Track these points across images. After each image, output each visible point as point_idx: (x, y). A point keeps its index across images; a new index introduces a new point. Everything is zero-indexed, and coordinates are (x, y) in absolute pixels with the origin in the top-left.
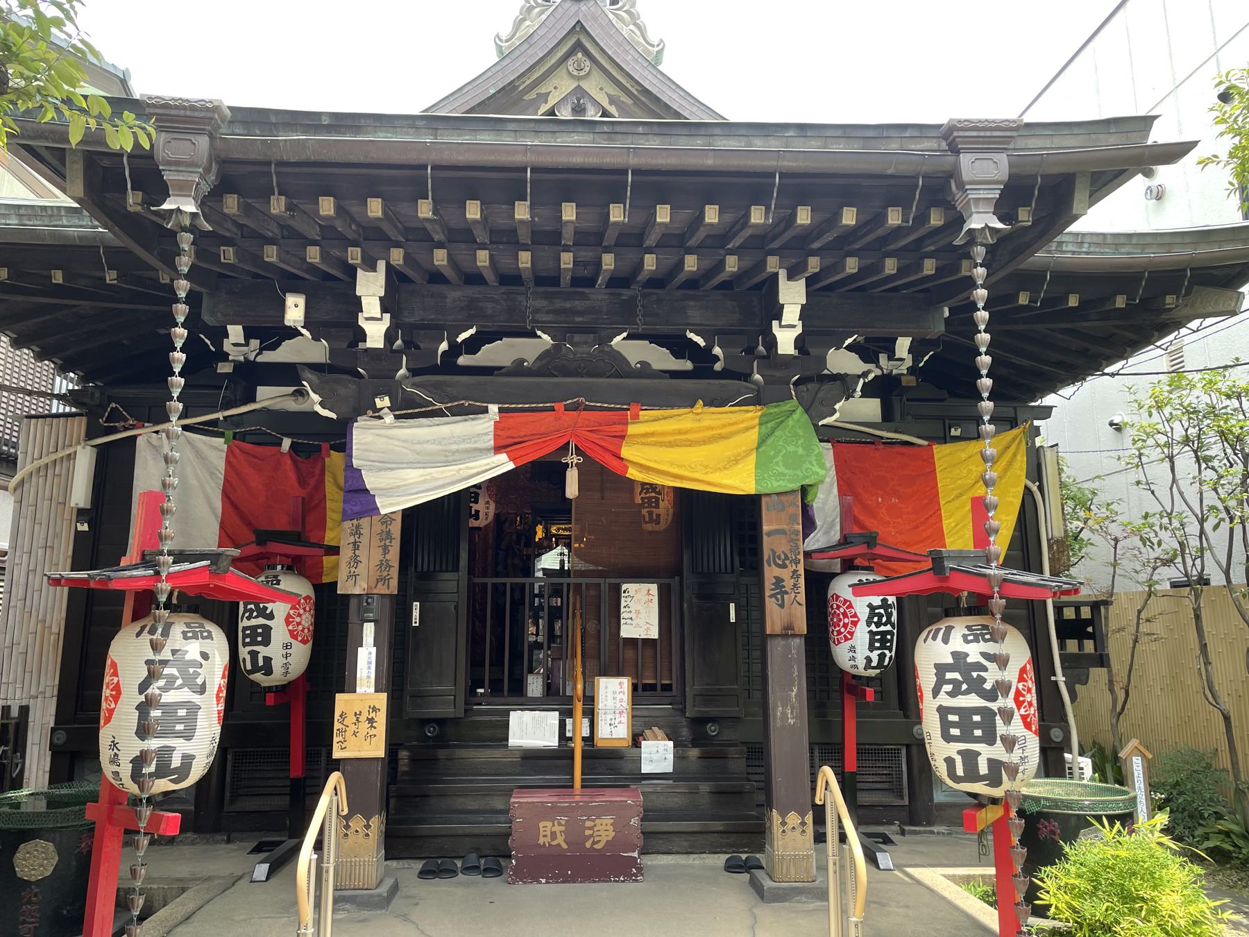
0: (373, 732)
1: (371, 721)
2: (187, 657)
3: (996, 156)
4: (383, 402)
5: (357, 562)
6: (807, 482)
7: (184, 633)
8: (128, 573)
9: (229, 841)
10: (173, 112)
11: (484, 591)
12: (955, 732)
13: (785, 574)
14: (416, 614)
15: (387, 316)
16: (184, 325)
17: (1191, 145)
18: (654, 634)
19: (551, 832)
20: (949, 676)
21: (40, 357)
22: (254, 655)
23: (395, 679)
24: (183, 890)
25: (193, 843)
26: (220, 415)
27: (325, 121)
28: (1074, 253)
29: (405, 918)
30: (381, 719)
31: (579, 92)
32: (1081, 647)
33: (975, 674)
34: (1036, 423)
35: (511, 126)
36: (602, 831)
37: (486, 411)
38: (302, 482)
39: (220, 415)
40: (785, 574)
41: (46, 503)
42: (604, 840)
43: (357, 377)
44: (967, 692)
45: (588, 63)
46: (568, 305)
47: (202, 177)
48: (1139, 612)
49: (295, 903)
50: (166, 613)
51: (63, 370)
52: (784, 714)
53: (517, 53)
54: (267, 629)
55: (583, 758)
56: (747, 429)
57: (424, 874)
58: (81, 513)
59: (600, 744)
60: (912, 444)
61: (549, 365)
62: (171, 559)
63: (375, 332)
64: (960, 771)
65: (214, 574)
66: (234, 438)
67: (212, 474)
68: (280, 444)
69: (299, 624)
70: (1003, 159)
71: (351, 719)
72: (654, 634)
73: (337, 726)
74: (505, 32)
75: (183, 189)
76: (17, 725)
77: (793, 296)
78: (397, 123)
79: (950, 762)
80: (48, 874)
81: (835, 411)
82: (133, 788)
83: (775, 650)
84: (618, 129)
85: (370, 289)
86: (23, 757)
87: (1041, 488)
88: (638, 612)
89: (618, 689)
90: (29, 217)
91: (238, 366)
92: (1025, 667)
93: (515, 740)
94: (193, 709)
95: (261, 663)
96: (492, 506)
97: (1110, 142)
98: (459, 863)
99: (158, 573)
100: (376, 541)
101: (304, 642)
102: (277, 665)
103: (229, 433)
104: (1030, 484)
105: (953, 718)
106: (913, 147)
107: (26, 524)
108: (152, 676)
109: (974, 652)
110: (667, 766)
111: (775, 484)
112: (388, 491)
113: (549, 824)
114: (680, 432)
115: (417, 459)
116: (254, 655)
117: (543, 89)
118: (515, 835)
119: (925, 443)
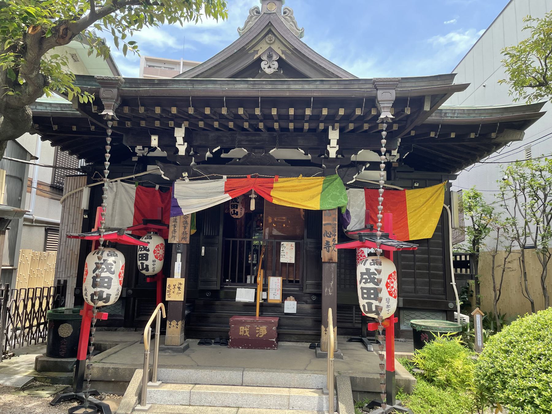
0: (180, 292)
1: (179, 288)
2: (108, 262)
3: (391, 91)
4: (185, 174)
5: (175, 232)
6: (340, 205)
7: (108, 254)
8: (93, 234)
9: (136, 331)
10: (106, 81)
11: (229, 243)
12: (365, 296)
13: (330, 240)
14: (203, 251)
15: (186, 144)
16: (109, 153)
17: (469, 84)
18: (293, 261)
19: (244, 331)
20: (364, 276)
21: (71, 154)
22: (142, 264)
23: (190, 274)
24: (117, 345)
25: (123, 331)
26: (133, 176)
27: (156, 82)
28: (451, 117)
29: (188, 356)
30: (183, 287)
31: (270, 49)
32: (461, 271)
33: (372, 276)
34: (450, 181)
35: (219, 82)
36: (263, 331)
37: (222, 178)
38: (163, 202)
39: (133, 176)
40: (330, 240)
41: (73, 207)
42: (263, 334)
43: (175, 164)
44: (369, 282)
45: (274, 38)
46: (253, 138)
47: (115, 102)
48: (505, 259)
49: (142, 342)
50: (103, 248)
51: (79, 158)
52: (328, 291)
53: (245, 35)
54: (147, 255)
55: (260, 306)
56: (318, 186)
57: (200, 343)
58: (85, 211)
59: (269, 301)
60: (398, 190)
61: (245, 161)
62: (104, 230)
63: (182, 149)
64: (367, 310)
65: (119, 235)
66: (139, 184)
67: (131, 198)
68: (155, 187)
69: (158, 253)
70: (393, 92)
71: (172, 287)
72: (293, 261)
73: (167, 289)
74: (242, 27)
75: (109, 107)
76: (63, 286)
77: (334, 136)
78: (180, 82)
79: (364, 306)
80: (69, 335)
81: (353, 179)
82: (92, 304)
83: (325, 267)
84: (256, 82)
85: (179, 134)
86: (65, 298)
87: (450, 208)
88: (287, 253)
89: (277, 281)
90: (64, 108)
91: (140, 158)
92: (391, 274)
93: (238, 299)
94: (110, 279)
95: (145, 267)
96: (243, 210)
97: (437, 85)
98: (213, 341)
99: (100, 235)
100: (182, 225)
101: (160, 260)
102: (150, 268)
103: (137, 183)
104: (445, 206)
105: (365, 291)
106: (363, 87)
107: (66, 215)
108: (97, 268)
109: (373, 269)
110: (294, 311)
111: (327, 206)
112: (187, 207)
113: (243, 328)
114: (293, 186)
115: (197, 195)
116: (142, 264)
117: (256, 49)
118: (231, 331)
119: (403, 189)
